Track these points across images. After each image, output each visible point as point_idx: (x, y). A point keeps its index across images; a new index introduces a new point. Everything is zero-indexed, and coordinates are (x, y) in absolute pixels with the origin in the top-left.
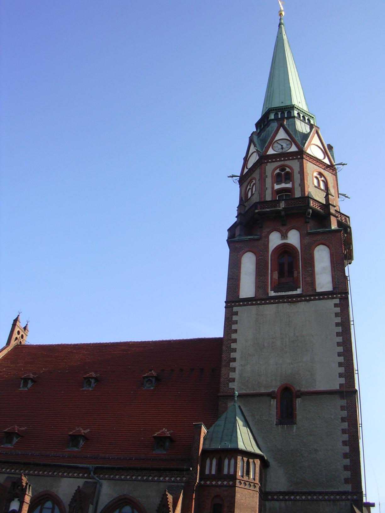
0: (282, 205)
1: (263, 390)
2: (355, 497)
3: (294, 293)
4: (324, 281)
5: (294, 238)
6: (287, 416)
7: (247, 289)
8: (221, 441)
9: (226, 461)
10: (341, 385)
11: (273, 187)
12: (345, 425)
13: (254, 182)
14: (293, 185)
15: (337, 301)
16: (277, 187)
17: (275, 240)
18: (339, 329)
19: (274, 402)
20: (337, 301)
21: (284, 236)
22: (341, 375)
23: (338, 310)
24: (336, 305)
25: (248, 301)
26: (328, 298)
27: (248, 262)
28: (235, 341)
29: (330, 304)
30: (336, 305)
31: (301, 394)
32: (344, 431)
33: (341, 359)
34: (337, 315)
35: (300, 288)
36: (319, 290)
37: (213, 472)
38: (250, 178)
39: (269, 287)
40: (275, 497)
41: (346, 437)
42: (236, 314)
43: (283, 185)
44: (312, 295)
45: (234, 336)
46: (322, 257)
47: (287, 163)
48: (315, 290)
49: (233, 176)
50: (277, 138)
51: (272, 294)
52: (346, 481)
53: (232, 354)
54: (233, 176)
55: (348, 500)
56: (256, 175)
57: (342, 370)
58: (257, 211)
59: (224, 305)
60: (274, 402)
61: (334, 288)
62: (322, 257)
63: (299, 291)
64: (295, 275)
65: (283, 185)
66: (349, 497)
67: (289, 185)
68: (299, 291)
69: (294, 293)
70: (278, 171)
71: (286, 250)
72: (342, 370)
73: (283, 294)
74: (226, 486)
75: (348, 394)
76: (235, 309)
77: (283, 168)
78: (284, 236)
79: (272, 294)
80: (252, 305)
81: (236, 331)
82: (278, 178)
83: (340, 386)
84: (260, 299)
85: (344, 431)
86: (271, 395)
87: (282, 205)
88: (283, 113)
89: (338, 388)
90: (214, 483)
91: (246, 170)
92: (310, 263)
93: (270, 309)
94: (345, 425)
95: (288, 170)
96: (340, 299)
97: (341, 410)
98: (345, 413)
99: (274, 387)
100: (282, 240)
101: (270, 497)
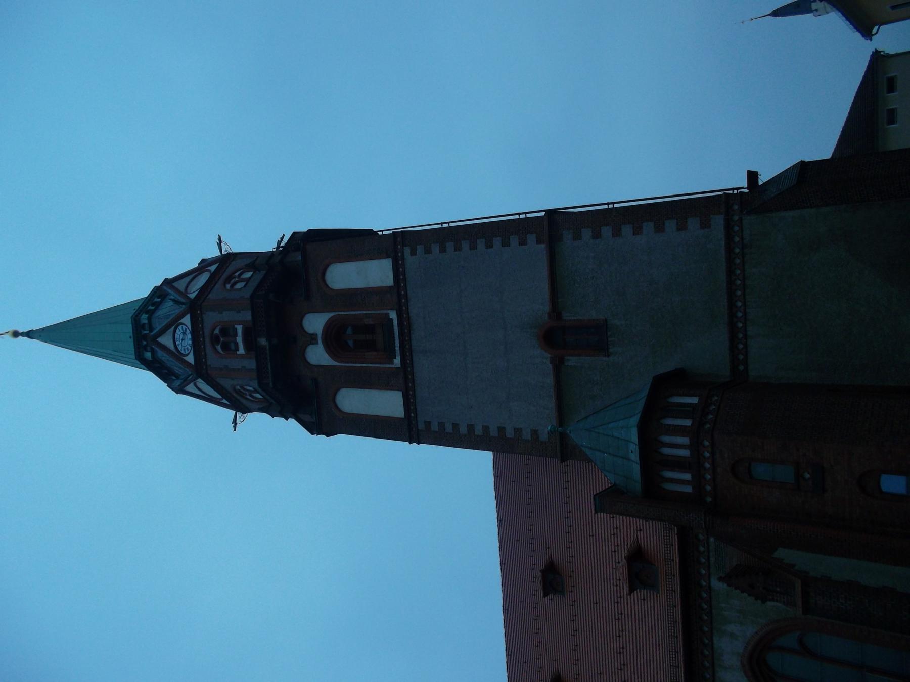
0: (263, 341)
1: (550, 380)
2: (736, 207)
3: (395, 323)
4: (376, 273)
5: (315, 323)
6: (596, 337)
7: (390, 403)
8: (629, 459)
9: (667, 451)
10: (539, 242)
11: (242, 356)
12: (606, 231)
13: (238, 388)
14: (239, 323)
15: (407, 250)
16: (241, 351)
17: (318, 355)
18: (450, 246)
19: (572, 361)
20: (407, 250)
21: (312, 339)
22: (523, 243)
23: (420, 249)
24: (413, 253)
25: (409, 403)
26: (404, 264)
27: (352, 400)
28: (501, 430)
29: (411, 262)
30: (413, 253)
31: (556, 311)
32: (617, 233)
33: (497, 242)
34: (428, 251)
35: (387, 315)
36: (389, 281)
37: (687, 477)
38: (235, 395)
39: (388, 366)
40: (741, 357)
41: (627, 230)
42: (428, 424)
43: (239, 339)
44: (398, 293)
45: (494, 432)
46: (344, 276)
47: (207, 332)
48: (390, 287)
49: (235, 422)
50: (172, 347)
51: (397, 362)
52: (705, 224)
53: (492, 434)
54: (235, 422)
55: (741, 220)
56: (227, 383)
57: (514, 240)
58: (271, 385)
59: (414, 444)
60: (572, 361)
61: (388, 257)
62: (344, 276)
63: (393, 315)
64: (370, 322)
65: (239, 339)
66: (736, 218)
67: (239, 329)
68: (393, 315)
69: (395, 323)
70: (219, 348)
71: (334, 339)
72: (514, 240)
73: (397, 348)
74: (713, 454)
75: (554, 226)
76: (421, 426)
77: (215, 340)
78: (312, 339)
79: (397, 362)
80: (414, 396)
81: (455, 426)
82: (229, 348)
83: (541, 243)
84: (405, 382)
85: (617, 233)
86: (558, 365)
87: (263, 341)
88: (145, 337)
89: (543, 246)
90: (708, 477)
91: (224, 401)
92: (352, 297)
93: (424, 368)
94: (606, 231)
95: (217, 331)
96: (404, 245)
97: (580, 239)
98: (587, 234)
99: (541, 358)
100: (317, 343)
101: (741, 368)
